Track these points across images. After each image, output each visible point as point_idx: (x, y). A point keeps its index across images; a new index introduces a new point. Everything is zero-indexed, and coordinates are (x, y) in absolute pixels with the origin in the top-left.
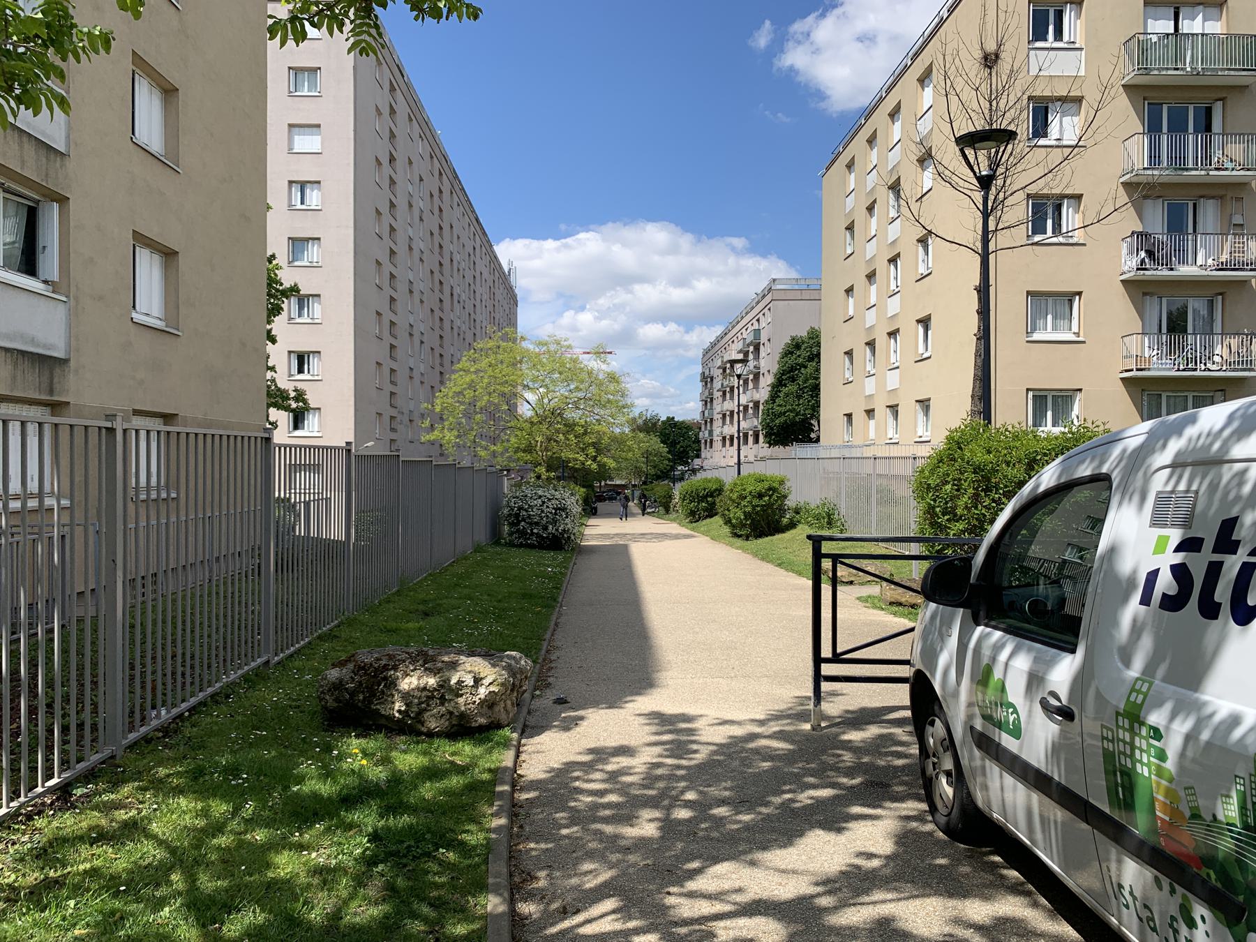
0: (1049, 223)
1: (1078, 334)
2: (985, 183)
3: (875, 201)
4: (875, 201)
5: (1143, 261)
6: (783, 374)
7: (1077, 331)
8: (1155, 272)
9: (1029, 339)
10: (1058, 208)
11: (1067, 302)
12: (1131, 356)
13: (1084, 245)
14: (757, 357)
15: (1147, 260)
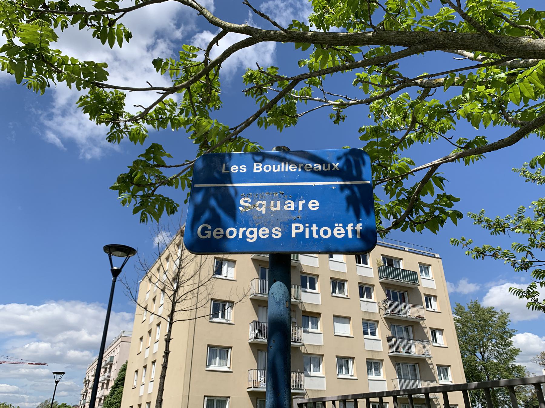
0: (220, 314)
1: (229, 368)
2: (116, 273)
3: (155, 297)
4: (155, 297)
5: (257, 334)
6: (119, 381)
7: (229, 366)
8: (261, 340)
9: (207, 369)
10: (224, 306)
11: (226, 351)
12: (251, 381)
13: (234, 324)
14: (110, 372)
15: (258, 334)
